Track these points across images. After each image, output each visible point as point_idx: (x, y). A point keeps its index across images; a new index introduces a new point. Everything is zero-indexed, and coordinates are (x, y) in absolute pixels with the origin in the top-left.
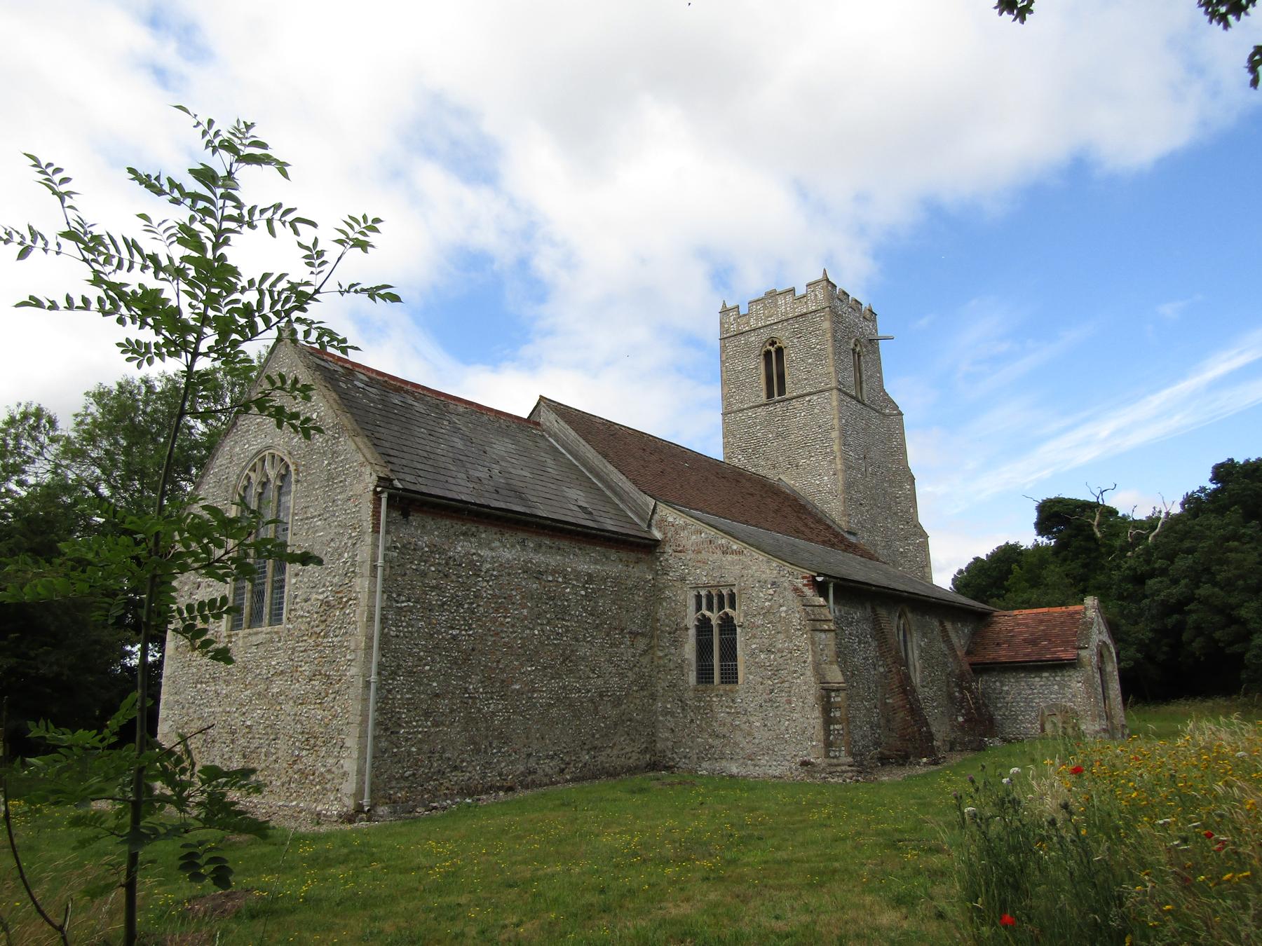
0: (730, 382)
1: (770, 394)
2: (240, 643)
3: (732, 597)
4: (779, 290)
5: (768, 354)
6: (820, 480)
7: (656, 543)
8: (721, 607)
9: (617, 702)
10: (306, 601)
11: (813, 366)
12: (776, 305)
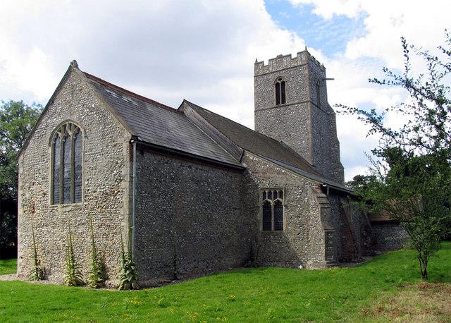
0: (259, 95)
1: (278, 103)
2: (59, 210)
3: (281, 193)
4: (283, 55)
5: (277, 85)
6: (301, 142)
7: (245, 169)
8: (275, 197)
9: (228, 238)
10: (95, 192)
11: (298, 91)
12: (282, 62)
